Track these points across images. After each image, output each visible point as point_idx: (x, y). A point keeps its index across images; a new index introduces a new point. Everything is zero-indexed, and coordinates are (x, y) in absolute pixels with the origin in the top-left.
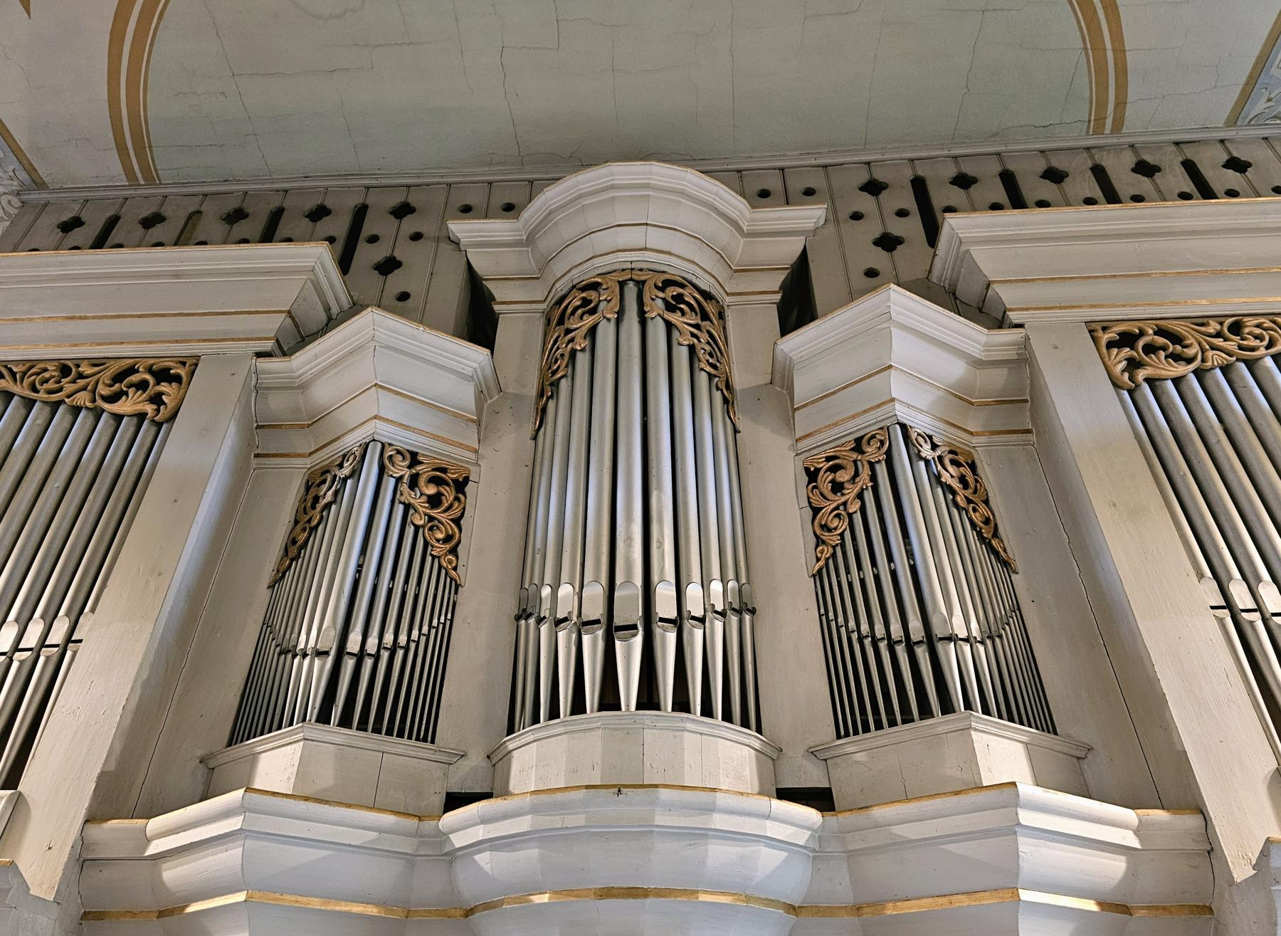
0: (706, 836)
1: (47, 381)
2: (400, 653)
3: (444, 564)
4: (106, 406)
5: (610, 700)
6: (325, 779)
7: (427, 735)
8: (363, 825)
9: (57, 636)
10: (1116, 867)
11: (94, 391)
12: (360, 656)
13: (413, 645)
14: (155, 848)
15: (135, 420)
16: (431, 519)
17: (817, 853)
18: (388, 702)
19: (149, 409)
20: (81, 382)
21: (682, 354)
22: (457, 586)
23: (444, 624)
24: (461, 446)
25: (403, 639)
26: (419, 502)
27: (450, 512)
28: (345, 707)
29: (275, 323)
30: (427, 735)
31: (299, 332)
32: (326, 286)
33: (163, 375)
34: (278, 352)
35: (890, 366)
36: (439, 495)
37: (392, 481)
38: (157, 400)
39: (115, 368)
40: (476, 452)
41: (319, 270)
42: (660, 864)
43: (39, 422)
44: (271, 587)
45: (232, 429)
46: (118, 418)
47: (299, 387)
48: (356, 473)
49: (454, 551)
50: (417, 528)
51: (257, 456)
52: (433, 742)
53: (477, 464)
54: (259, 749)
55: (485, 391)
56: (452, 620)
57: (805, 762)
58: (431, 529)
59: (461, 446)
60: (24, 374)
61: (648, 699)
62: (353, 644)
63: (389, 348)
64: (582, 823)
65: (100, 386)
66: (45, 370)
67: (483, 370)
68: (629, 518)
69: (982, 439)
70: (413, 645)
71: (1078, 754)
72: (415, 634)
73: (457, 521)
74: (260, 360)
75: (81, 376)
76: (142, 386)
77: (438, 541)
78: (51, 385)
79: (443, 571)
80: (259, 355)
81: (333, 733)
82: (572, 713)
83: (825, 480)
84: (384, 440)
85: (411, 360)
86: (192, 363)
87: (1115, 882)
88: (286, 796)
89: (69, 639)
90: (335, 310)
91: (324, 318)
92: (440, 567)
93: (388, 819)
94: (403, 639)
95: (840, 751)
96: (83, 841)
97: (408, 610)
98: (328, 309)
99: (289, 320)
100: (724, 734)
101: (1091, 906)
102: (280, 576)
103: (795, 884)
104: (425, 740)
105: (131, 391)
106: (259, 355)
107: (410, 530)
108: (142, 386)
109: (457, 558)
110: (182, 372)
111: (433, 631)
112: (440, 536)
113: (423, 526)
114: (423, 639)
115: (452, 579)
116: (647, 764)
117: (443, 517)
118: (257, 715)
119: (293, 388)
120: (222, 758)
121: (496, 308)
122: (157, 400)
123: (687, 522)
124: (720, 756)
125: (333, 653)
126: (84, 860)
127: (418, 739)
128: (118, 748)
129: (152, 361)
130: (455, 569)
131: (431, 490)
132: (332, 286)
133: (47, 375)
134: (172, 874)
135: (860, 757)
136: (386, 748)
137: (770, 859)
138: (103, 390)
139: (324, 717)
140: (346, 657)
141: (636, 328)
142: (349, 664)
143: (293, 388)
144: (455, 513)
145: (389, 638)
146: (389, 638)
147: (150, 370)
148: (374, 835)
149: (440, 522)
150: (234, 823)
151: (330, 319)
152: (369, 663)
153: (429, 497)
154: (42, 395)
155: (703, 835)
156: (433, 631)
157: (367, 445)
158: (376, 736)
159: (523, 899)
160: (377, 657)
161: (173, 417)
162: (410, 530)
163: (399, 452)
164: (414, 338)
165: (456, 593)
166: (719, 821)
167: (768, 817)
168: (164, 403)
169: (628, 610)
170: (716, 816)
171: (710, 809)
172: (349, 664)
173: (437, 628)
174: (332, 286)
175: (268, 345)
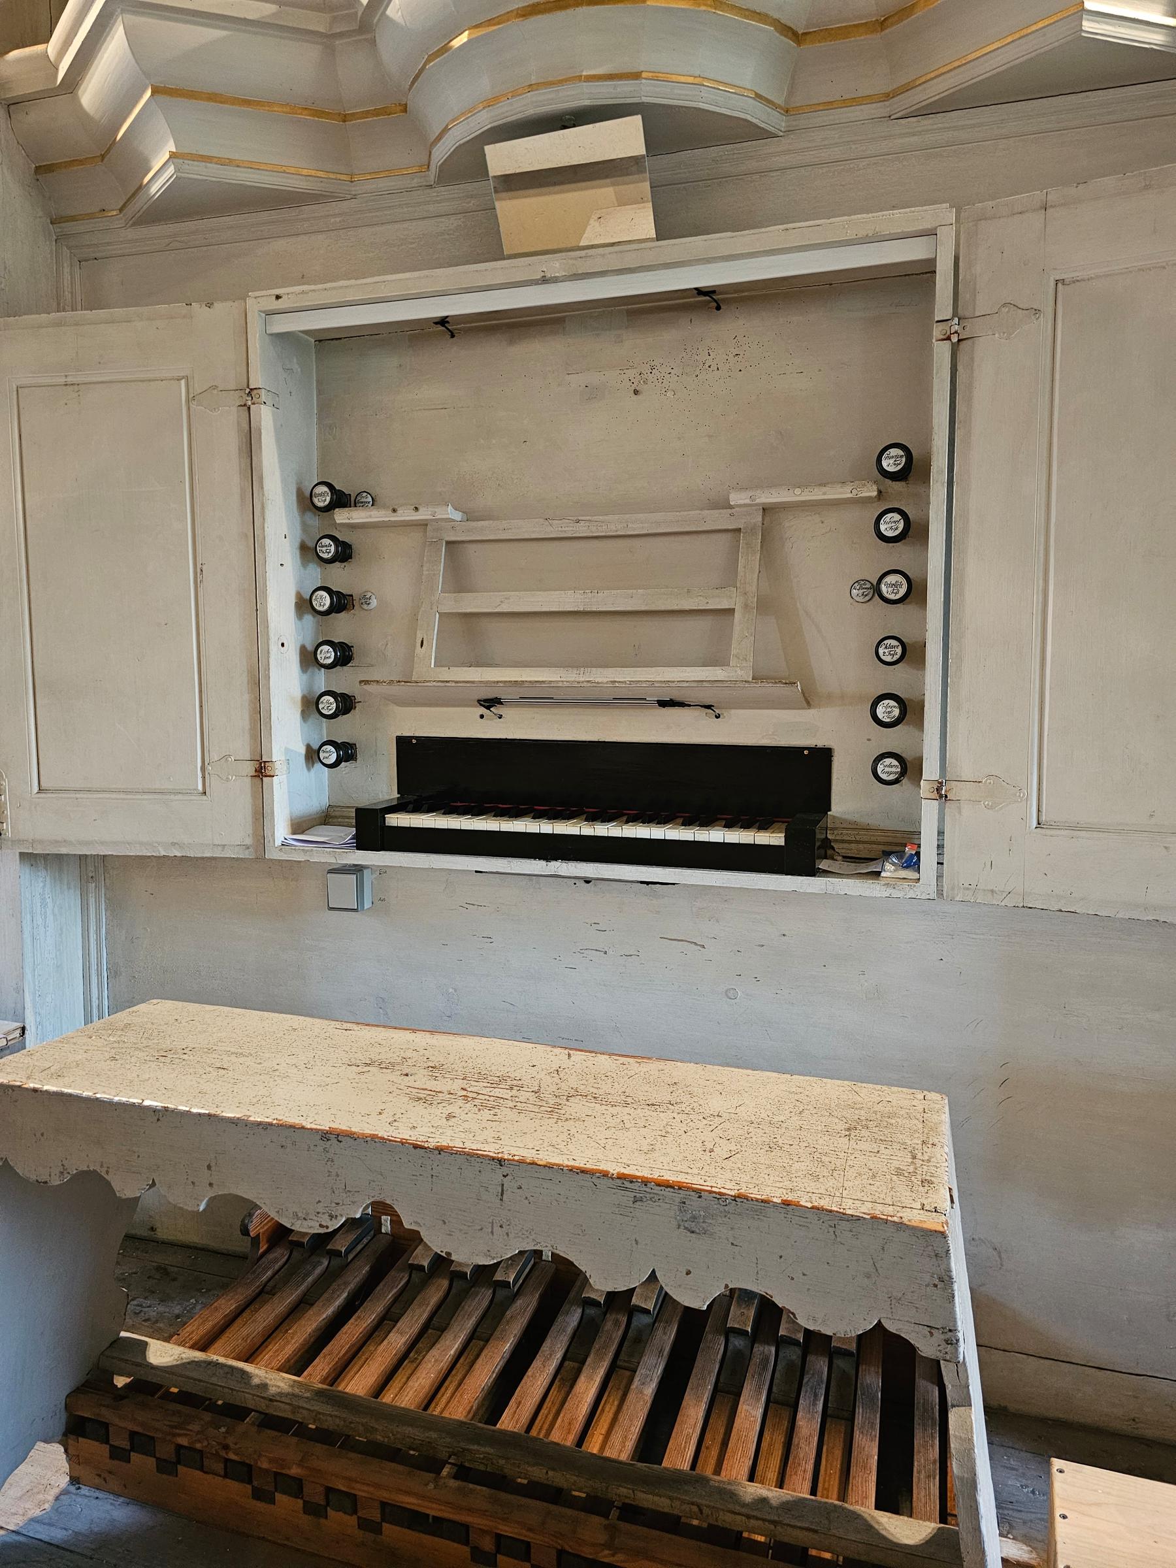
159: (445, 49)
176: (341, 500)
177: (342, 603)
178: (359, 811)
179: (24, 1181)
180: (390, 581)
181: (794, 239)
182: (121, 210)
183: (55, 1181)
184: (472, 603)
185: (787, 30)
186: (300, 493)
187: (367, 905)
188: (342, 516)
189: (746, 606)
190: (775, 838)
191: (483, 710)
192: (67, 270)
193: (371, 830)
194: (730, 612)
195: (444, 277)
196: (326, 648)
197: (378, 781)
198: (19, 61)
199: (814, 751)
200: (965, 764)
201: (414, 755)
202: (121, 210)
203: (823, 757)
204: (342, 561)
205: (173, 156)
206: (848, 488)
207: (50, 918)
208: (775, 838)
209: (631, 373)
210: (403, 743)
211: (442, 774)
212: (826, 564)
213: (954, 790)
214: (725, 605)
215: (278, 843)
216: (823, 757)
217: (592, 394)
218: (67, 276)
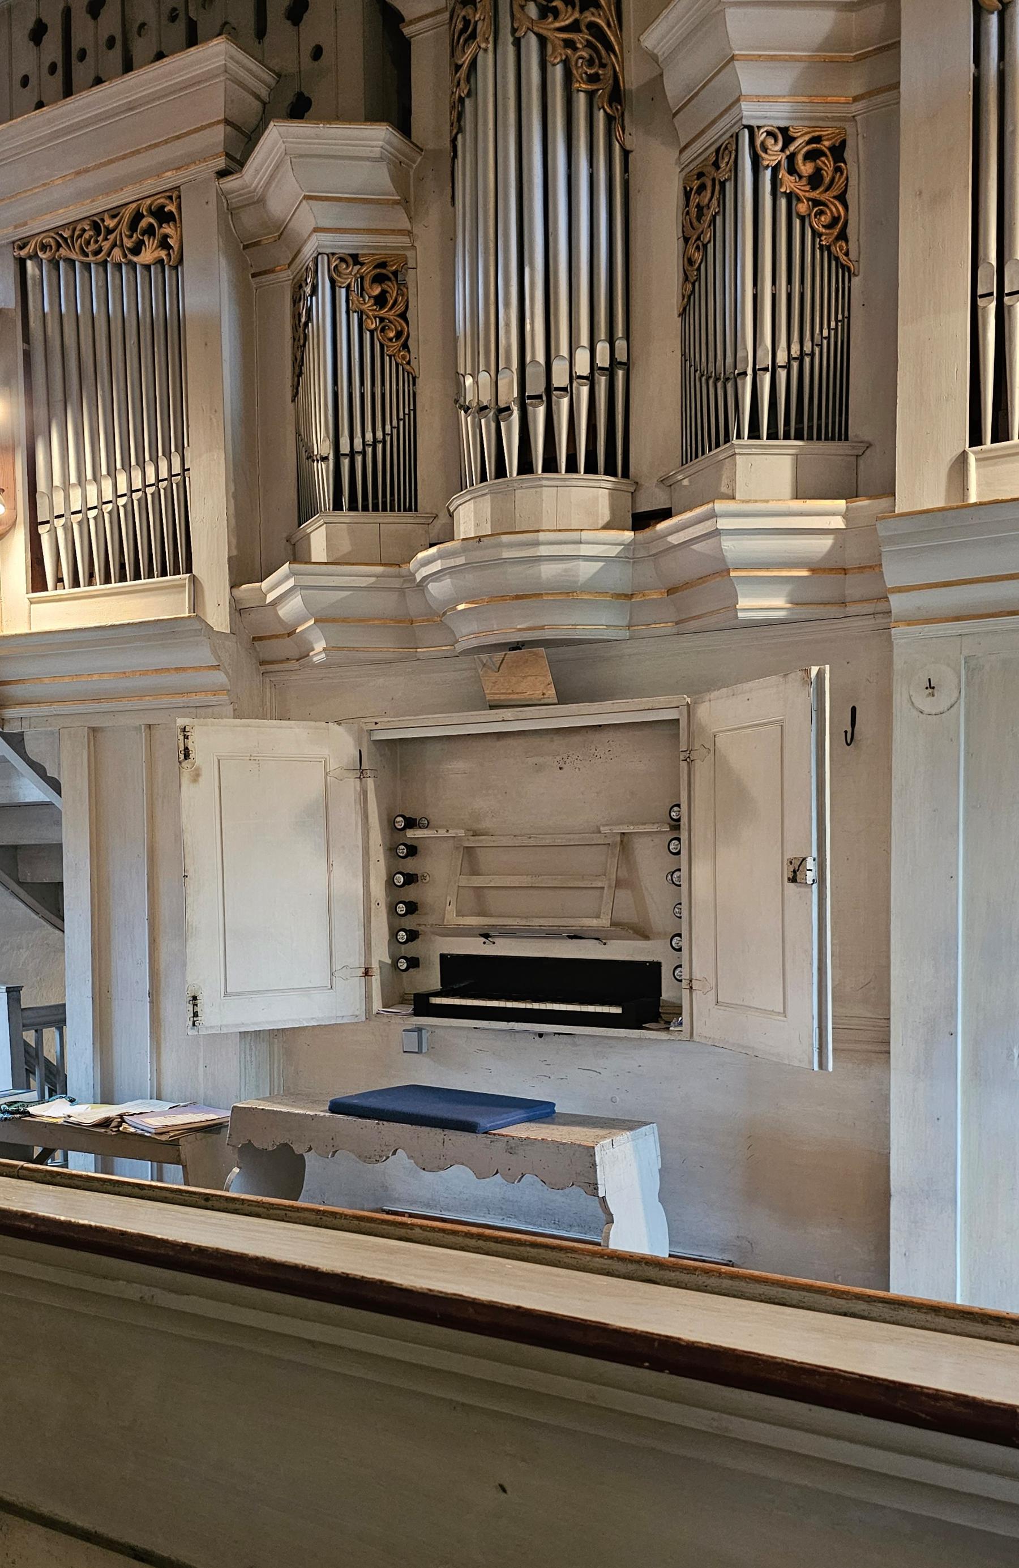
0: (539, 560)
1: (88, 243)
2: (380, 446)
3: (399, 361)
4: (135, 259)
5: (501, 472)
6: (345, 546)
7: (411, 507)
8: (363, 575)
9: (176, 469)
10: (826, 543)
11: (122, 245)
12: (352, 455)
13: (388, 438)
14: (270, 598)
15: (159, 266)
16: (382, 320)
17: (630, 556)
18: (383, 486)
19: (163, 254)
20: (111, 237)
21: (557, 73)
22: (414, 379)
23: (409, 415)
24: (393, 232)
25: (379, 435)
26: (368, 305)
27: (396, 308)
28: (351, 497)
29: (219, 133)
30: (411, 507)
31: (242, 132)
32: (242, 74)
33: (163, 216)
34: (234, 165)
35: (733, 58)
36: (384, 292)
37: (343, 291)
38: (164, 244)
39: (127, 214)
40: (409, 233)
41: (232, 65)
42: (515, 577)
43: (100, 284)
44: (293, 401)
45: (223, 262)
46: (147, 267)
47: (258, 202)
48: (314, 290)
49: (405, 346)
50: (372, 332)
51: (254, 276)
52: (416, 510)
53: (413, 247)
54: (309, 531)
55: (402, 158)
56: (415, 410)
57: (657, 490)
58: (383, 330)
59: (393, 232)
60: (72, 237)
61: (526, 467)
62: (345, 448)
63: (301, 156)
64: (464, 562)
65: (125, 240)
66: (84, 231)
67: (389, 143)
68: (507, 305)
69: (859, 106)
70: (388, 438)
71: (855, 452)
72: (388, 428)
73: (403, 316)
74: (222, 181)
75: (109, 231)
76: (150, 231)
77: (391, 340)
78: (93, 247)
79: (400, 368)
80: (222, 174)
81: (346, 516)
82: (497, 477)
83: (695, 200)
84: (328, 251)
85: (326, 161)
86: (174, 194)
87: (821, 555)
88: (326, 563)
89: (184, 470)
90: (264, 92)
91: (256, 105)
92: (397, 365)
93: (380, 569)
94: (379, 435)
95: (675, 480)
96: (234, 601)
97: (380, 406)
98: (258, 97)
99: (229, 128)
100: (574, 483)
101: (805, 573)
102: (295, 394)
103: (620, 578)
104: (410, 510)
105: (146, 238)
106: (222, 174)
107: (367, 336)
108: (150, 231)
109: (409, 352)
110: (171, 208)
111: (401, 423)
112: (392, 335)
113: (376, 329)
114: (395, 431)
115: (408, 374)
116: (518, 515)
117: (391, 315)
118: (306, 510)
119: (254, 203)
120: (300, 535)
121: (407, 31)
122: (164, 244)
123: (556, 293)
124: (592, 496)
125: (331, 457)
126: (238, 610)
127: (405, 510)
128: (234, 541)
129: (149, 201)
130: (409, 363)
131: (377, 291)
132: (249, 71)
133: (86, 236)
134: (730, 546)
135: (686, 482)
136: (380, 520)
137: (586, 570)
138: (128, 243)
139: (337, 506)
140: (342, 458)
141: (511, 50)
142: (346, 462)
143: (254, 203)
144: (400, 308)
145: (369, 436)
146: (369, 436)
147: (152, 213)
148: (373, 579)
149: (390, 322)
150: (290, 583)
151: (264, 104)
152: (359, 459)
153: (376, 298)
154: (91, 258)
155: (539, 559)
156: (401, 423)
157: (317, 258)
158: (366, 513)
159: (454, 608)
160: (364, 453)
161: (181, 261)
162: (367, 336)
163: (342, 260)
164: (318, 137)
165: (414, 384)
166: (543, 551)
167: (581, 543)
168: (172, 247)
169: (509, 392)
170: (542, 548)
171: (537, 544)
172: (346, 462)
173: (404, 420)
174: (249, 71)
175: (221, 163)
176: (411, 823)
177: (411, 879)
178: (415, 995)
179: (257, 1149)
180: (440, 871)
181: (616, 708)
182: (290, 265)
183: (270, 1149)
184: (478, 881)
185: (618, 596)
186: (389, 821)
187: (424, 1050)
188: (410, 833)
189: (610, 886)
190: (618, 1010)
191: (483, 940)
192: (268, 690)
193: (422, 1006)
194: (603, 888)
195: (456, 717)
196: (401, 905)
197: (431, 978)
198: (245, 590)
199: (652, 963)
200: (697, 974)
201: (450, 963)
202: (290, 265)
203: (657, 966)
204: (412, 856)
205: (324, 649)
206: (656, 826)
207: (253, 1059)
208: (618, 1010)
209: (558, 758)
210: (443, 957)
211: (466, 975)
212: (650, 859)
213: (695, 985)
214: (600, 885)
215: (374, 1012)
216: (657, 966)
217: (539, 768)
218: (268, 694)
